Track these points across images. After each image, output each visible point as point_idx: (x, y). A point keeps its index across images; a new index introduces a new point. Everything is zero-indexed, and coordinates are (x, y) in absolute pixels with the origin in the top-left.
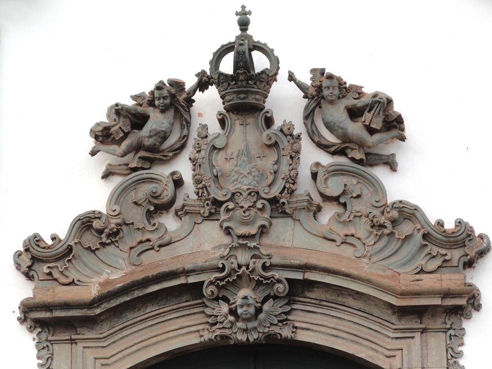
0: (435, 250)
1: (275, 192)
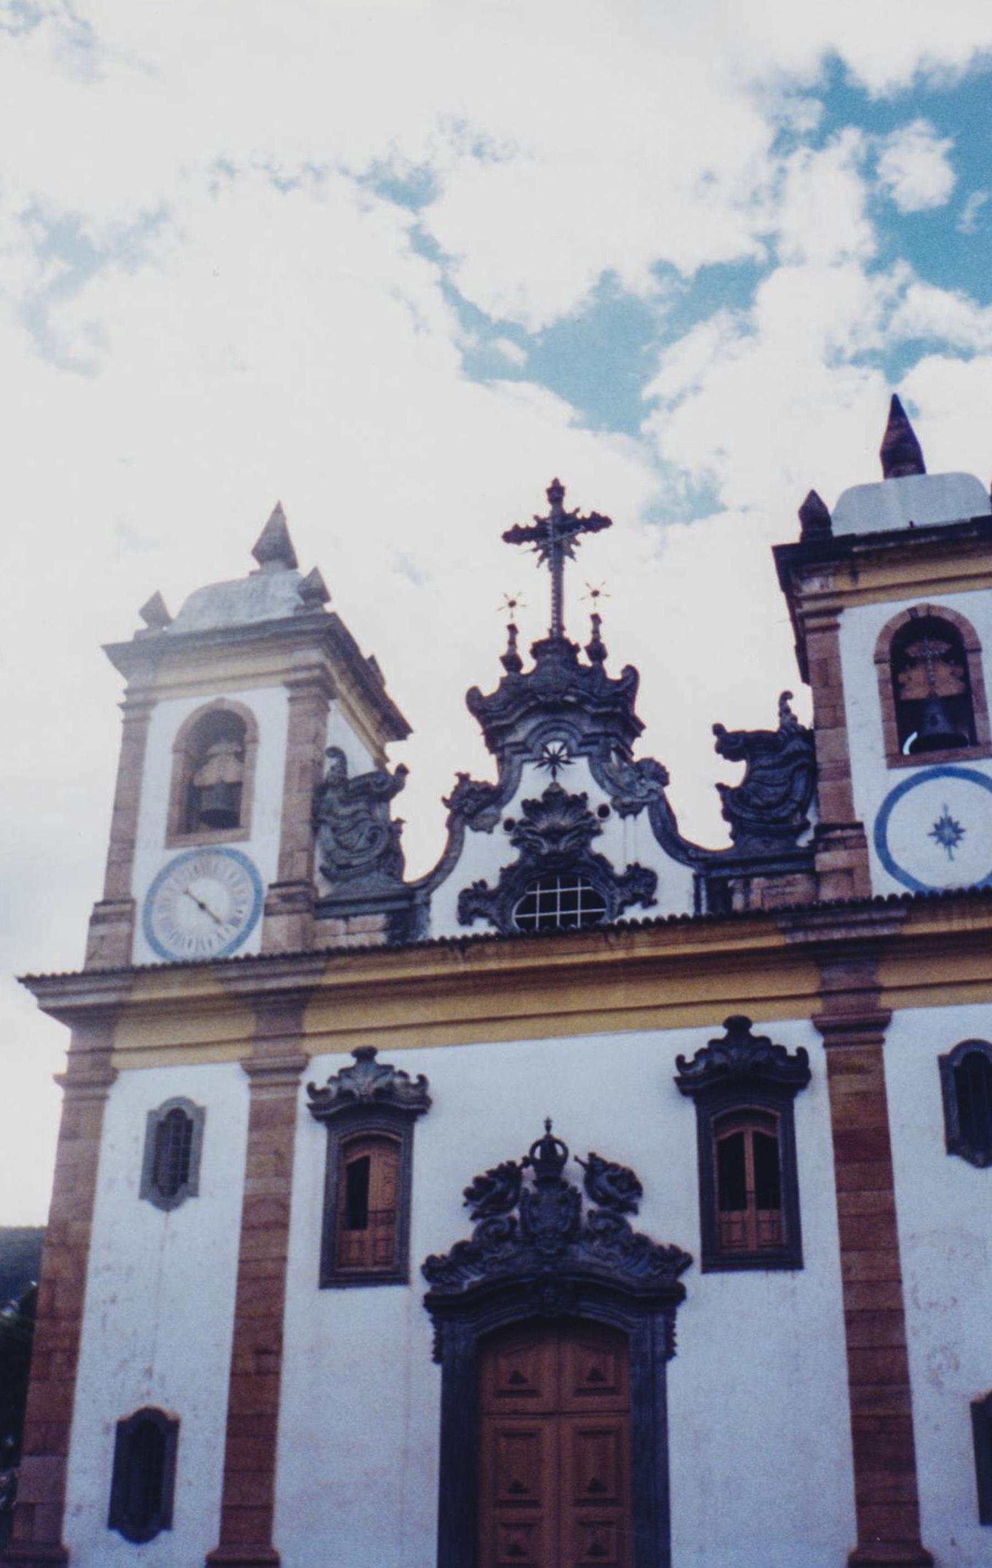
0: (658, 1263)
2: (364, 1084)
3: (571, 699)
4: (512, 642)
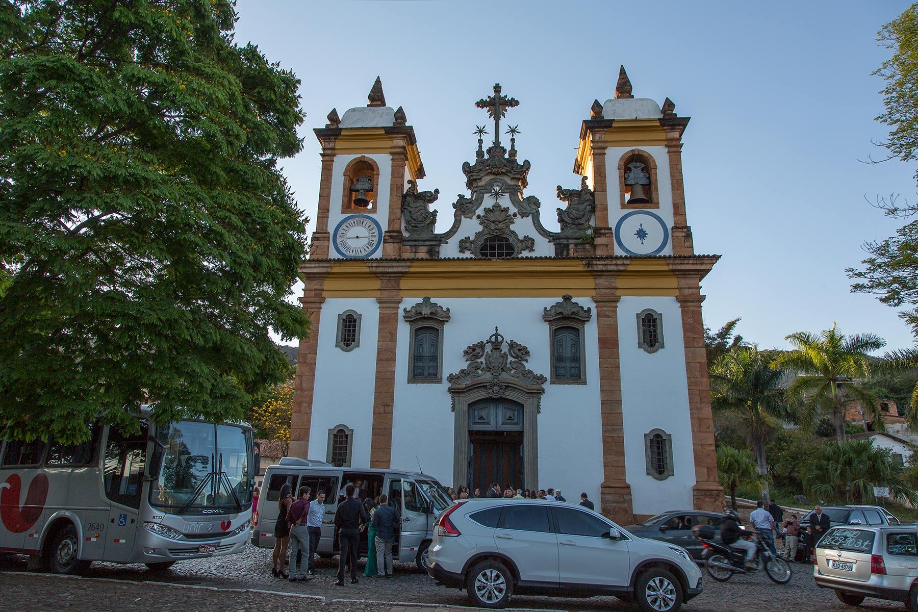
1: (502, 367)
2: (426, 311)
3: (504, 171)
4: (480, 147)
